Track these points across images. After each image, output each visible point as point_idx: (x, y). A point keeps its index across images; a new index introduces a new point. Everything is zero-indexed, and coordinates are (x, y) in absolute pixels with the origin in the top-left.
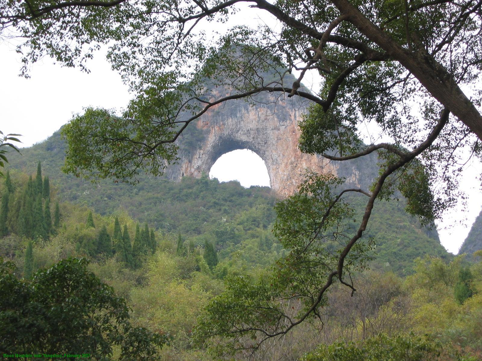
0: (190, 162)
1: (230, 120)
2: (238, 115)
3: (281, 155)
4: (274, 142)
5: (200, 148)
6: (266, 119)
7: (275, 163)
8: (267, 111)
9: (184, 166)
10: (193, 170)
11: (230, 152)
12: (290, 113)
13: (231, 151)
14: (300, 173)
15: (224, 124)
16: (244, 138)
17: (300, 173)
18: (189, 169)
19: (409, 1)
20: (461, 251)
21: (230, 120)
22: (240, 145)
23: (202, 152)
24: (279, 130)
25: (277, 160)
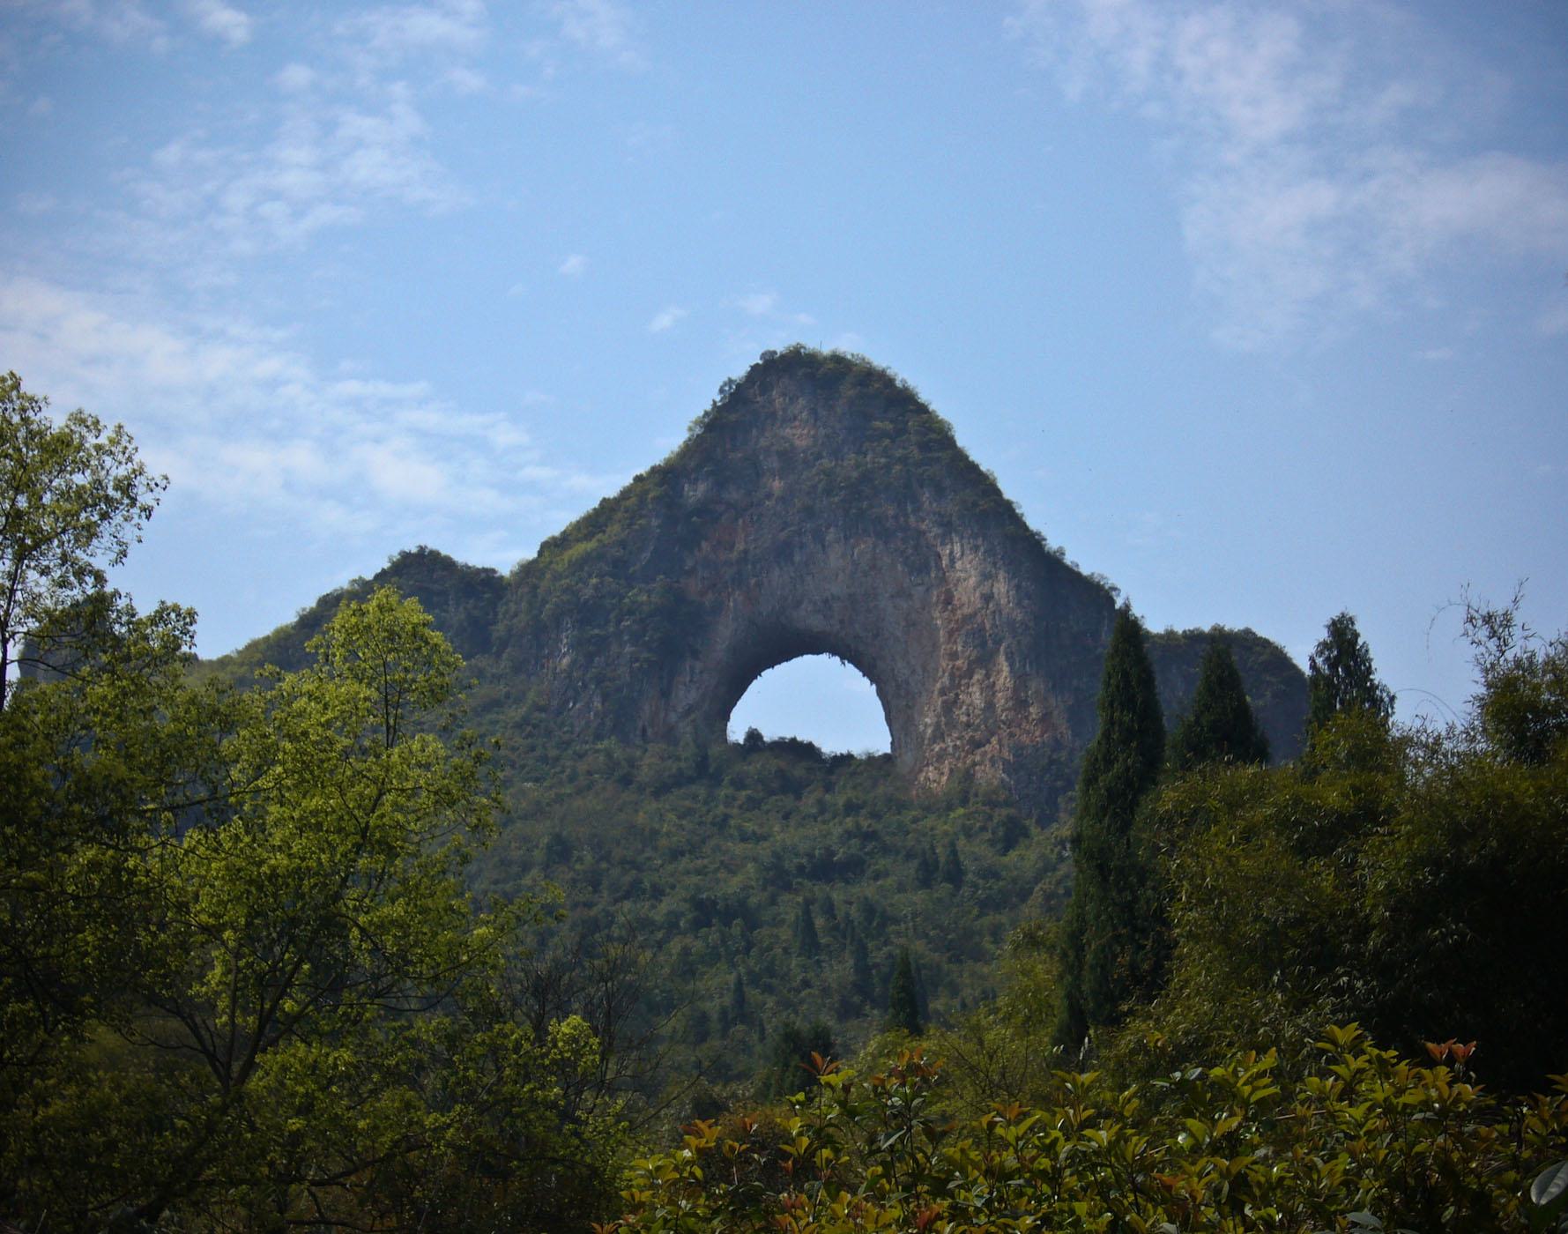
0: (665, 694)
1: (777, 572)
2: (797, 558)
3: (920, 671)
4: (899, 634)
5: (695, 654)
6: (873, 567)
7: (902, 693)
8: (875, 547)
9: (646, 707)
10: (673, 717)
11: (785, 664)
12: (939, 549)
13: (788, 660)
14: (964, 719)
15: (759, 585)
16: (816, 623)
17: (964, 719)
18: (662, 715)
19: (5, 950)
20: (285, 650)
21: (777, 572)
22: (814, 645)
23: (698, 666)
24: (910, 596)
25: (908, 683)
